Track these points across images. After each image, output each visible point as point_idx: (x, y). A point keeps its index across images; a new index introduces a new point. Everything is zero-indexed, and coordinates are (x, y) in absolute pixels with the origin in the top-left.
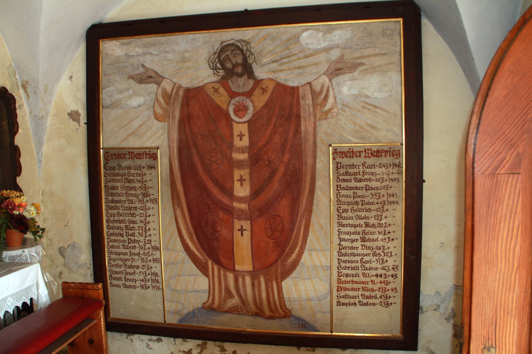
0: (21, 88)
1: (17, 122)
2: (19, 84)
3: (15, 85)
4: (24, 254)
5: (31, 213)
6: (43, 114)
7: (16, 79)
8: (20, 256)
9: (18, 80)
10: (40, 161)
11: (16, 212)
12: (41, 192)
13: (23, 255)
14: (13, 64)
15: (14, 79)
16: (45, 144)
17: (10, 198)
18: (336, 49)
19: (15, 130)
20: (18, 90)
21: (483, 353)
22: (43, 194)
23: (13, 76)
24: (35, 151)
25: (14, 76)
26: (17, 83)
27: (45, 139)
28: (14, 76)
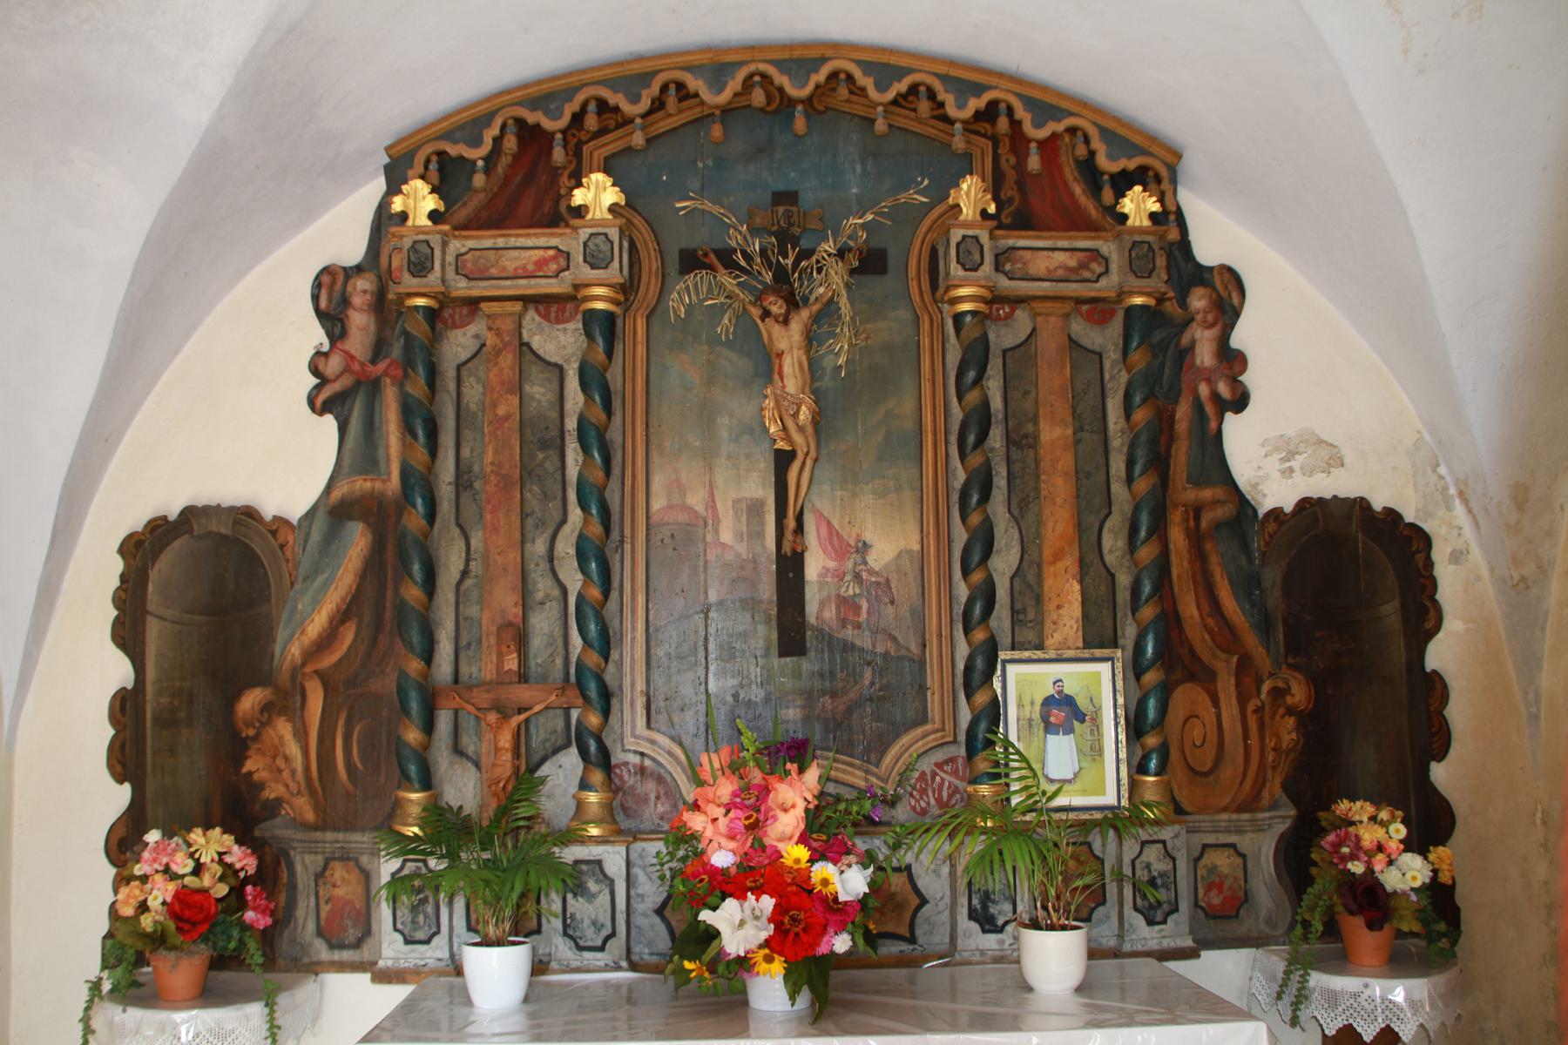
0: (1457, 502)
1: (1435, 603)
2: (1453, 491)
3: (1438, 496)
4: (1367, 992)
5: (1408, 876)
6: (1526, 572)
7: (1441, 477)
8: (1356, 995)
9: (1448, 479)
10: (1534, 718)
11: (1357, 868)
12: (1539, 815)
13: (1364, 996)
14: (1427, 437)
15: (1434, 479)
16: (1545, 666)
17: (1352, 823)
18: (1225, 426)
19: (1430, 624)
20: (1449, 509)
21: (274, 1041)
22: (1544, 823)
23: (1429, 470)
24: (1516, 687)
25: (1434, 471)
26: (1445, 489)
27: (1546, 647)
28: (1434, 471)
